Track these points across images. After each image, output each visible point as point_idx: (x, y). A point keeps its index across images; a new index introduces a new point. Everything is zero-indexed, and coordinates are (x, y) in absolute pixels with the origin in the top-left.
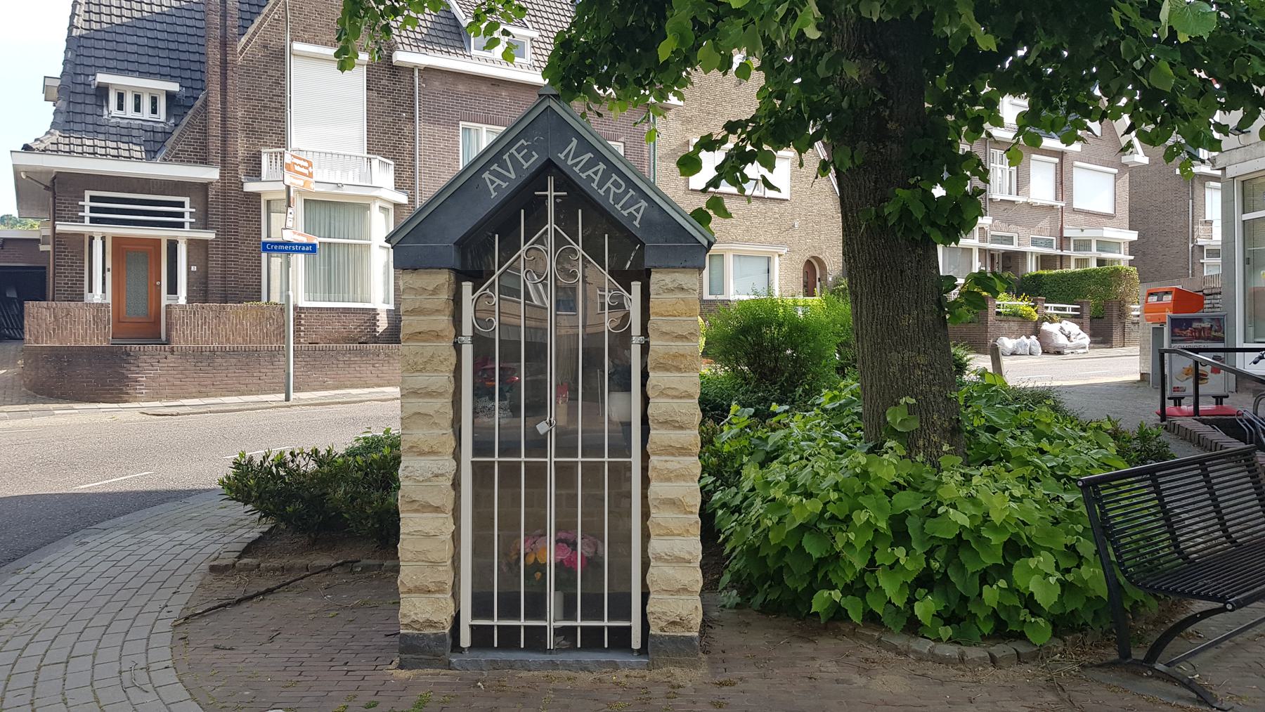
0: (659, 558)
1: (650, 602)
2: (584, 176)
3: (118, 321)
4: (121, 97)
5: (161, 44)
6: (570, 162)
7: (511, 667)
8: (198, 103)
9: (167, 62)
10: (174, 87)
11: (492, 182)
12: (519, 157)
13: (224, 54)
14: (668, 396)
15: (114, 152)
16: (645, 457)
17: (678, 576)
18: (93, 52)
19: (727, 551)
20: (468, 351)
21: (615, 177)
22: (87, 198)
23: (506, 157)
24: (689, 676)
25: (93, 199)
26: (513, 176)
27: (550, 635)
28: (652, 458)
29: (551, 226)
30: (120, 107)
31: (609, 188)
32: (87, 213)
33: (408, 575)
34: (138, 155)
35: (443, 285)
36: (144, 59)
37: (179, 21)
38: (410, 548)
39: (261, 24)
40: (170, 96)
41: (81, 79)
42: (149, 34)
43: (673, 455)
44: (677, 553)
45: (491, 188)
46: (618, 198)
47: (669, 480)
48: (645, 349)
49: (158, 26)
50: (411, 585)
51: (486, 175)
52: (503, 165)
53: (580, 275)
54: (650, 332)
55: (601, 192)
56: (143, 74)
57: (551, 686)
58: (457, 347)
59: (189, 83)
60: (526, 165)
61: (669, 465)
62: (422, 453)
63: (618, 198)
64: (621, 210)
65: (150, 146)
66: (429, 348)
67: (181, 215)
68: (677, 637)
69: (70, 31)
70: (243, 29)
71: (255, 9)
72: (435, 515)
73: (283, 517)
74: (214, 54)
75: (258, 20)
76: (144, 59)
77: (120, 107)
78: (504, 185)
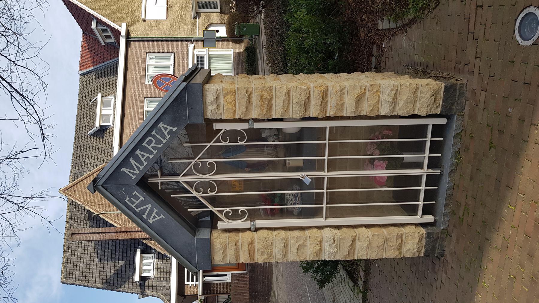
1: (420, 114)
2: (145, 163)
6: (137, 172)
9: (128, 253)
10: (138, 252)
12: (137, 203)
14: (288, 106)
17: (405, 98)
20: (259, 223)
21: (144, 144)
22: (188, 283)
23: (138, 210)
25: (188, 281)
27: (431, 172)
29: (180, 179)
31: (153, 147)
37: (110, 248)
38: (376, 253)
43: (327, 101)
45: (158, 218)
46: (158, 142)
47: (343, 104)
51: (151, 221)
54: (246, 118)
55: (155, 152)
59: (137, 245)
60: (142, 198)
61: (333, 105)
62: (321, 250)
63: (158, 142)
67: (193, 280)
68: (444, 97)
70: (111, 226)
71: (101, 222)
72: (357, 241)
78: (156, 210)
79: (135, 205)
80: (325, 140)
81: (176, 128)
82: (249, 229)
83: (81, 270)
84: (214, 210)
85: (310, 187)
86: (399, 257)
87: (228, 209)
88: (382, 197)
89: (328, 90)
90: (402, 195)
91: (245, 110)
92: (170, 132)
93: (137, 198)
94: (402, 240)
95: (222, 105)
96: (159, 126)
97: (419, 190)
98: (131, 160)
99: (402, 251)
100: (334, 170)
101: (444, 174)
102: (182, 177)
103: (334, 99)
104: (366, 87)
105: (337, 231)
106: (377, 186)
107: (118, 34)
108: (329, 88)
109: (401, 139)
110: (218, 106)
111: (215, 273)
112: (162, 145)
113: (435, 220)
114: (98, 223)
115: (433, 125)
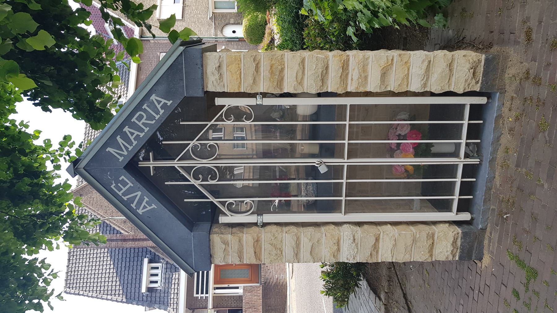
0: (425, 85)
2: (135, 143)
3: (251, 281)
4: (152, 282)
5: (128, 265)
6: (125, 153)
7: (490, 189)
8: (153, 250)
10: (146, 260)
11: (145, 207)
12: (124, 189)
13: (129, 240)
14: (302, 78)
15: (176, 285)
16: (348, 94)
17: (440, 70)
18: (133, 293)
19: (407, 23)
20: (268, 218)
21: (134, 120)
23: (125, 198)
24: (516, 64)
25: (197, 293)
26: (139, 193)
27: (470, 161)
28: (349, 90)
29: (176, 164)
30: (156, 282)
31: (143, 124)
32: (204, 295)
33: (420, 256)
34: (177, 275)
35: (221, 238)
36: (135, 272)
39: (114, 224)
40: (150, 262)
41: (145, 298)
42: (123, 269)
43: (347, 74)
44: (423, 71)
45: (149, 208)
47: (366, 78)
48: (264, 95)
49: (120, 266)
50: (428, 255)
51: (140, 211)
52: (132, 200)
53: (212, 143)
54: (253, 92)
55: (146, 130)
56: (141, 272)
57: (512, 166)
58: (265, 225)
59: (144, 253)
60: (130, 184)
61: (355, 77)
62: (339, 250)
64: (160, 115)
65: (173, 270)
66: (265, 246)
69: (124, 302)
71: (108, 228)
72: (381, 241)
73: (359, 275)
74: (130, 244)
75: (113, 226)
76: (135, 272)
77: (156, 282)
78: (146, 199)
79: (122, 192)
80: (341, 196)
81: (171, 101)
82: (256, 224)
83: (85, 280)
84: (215, 201)
85: (326, 176)
86: (429, 260)
87: (231, 200)
88: (408, 189)
89: (349, 60)
90: (432, 188)
91: (252, 81)
92: (164, 106)
93: (125, 184)
94: (433, 240)
95: (225, 76)
96: (151, 98)
97: (454, 183)
98: (118, 138)
99: (434, 253)
100: (356, 157)
101: (483, 163)
102: (179, 160)
103: (356, 71)
104: (393, 57)
105: (358, 228)
106: (409, 166)
107: (132, 33)
108: (351, 58)
109: (434, 120)
110: (221, 76)
111: (226, 286)
112: (154, 121)
113: (472, 218)
114: (105, 229)
115: (471, 105)
